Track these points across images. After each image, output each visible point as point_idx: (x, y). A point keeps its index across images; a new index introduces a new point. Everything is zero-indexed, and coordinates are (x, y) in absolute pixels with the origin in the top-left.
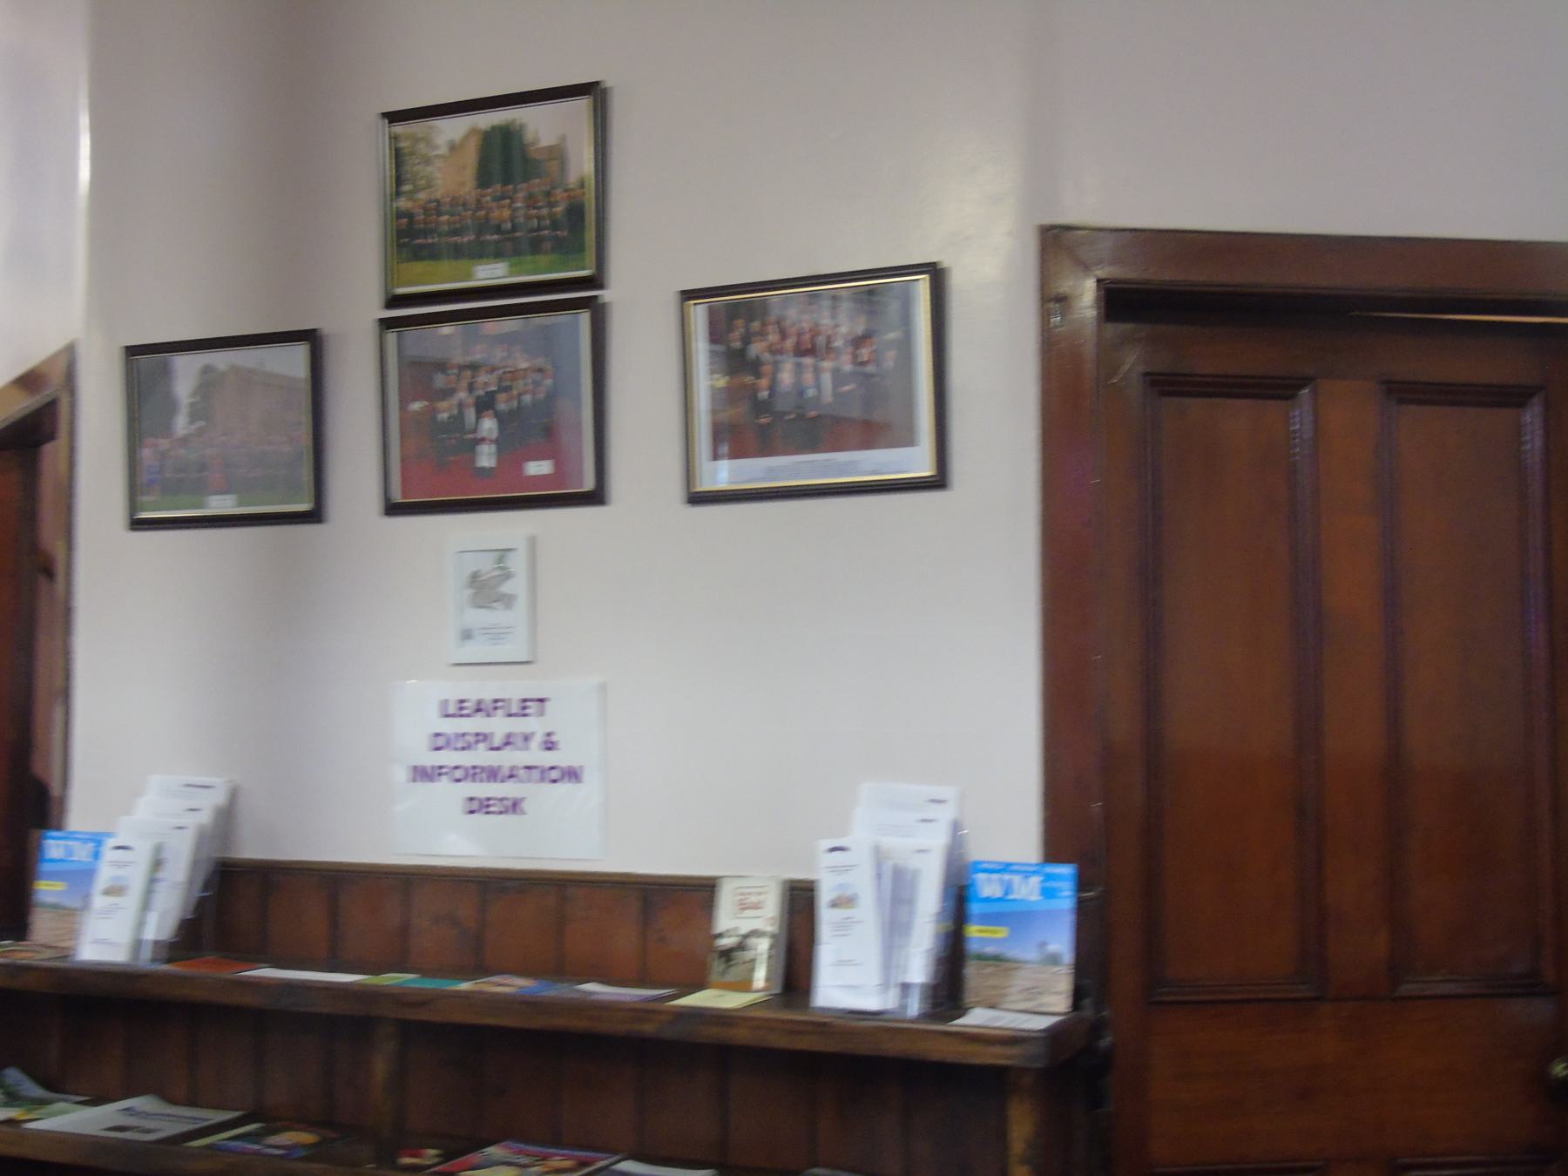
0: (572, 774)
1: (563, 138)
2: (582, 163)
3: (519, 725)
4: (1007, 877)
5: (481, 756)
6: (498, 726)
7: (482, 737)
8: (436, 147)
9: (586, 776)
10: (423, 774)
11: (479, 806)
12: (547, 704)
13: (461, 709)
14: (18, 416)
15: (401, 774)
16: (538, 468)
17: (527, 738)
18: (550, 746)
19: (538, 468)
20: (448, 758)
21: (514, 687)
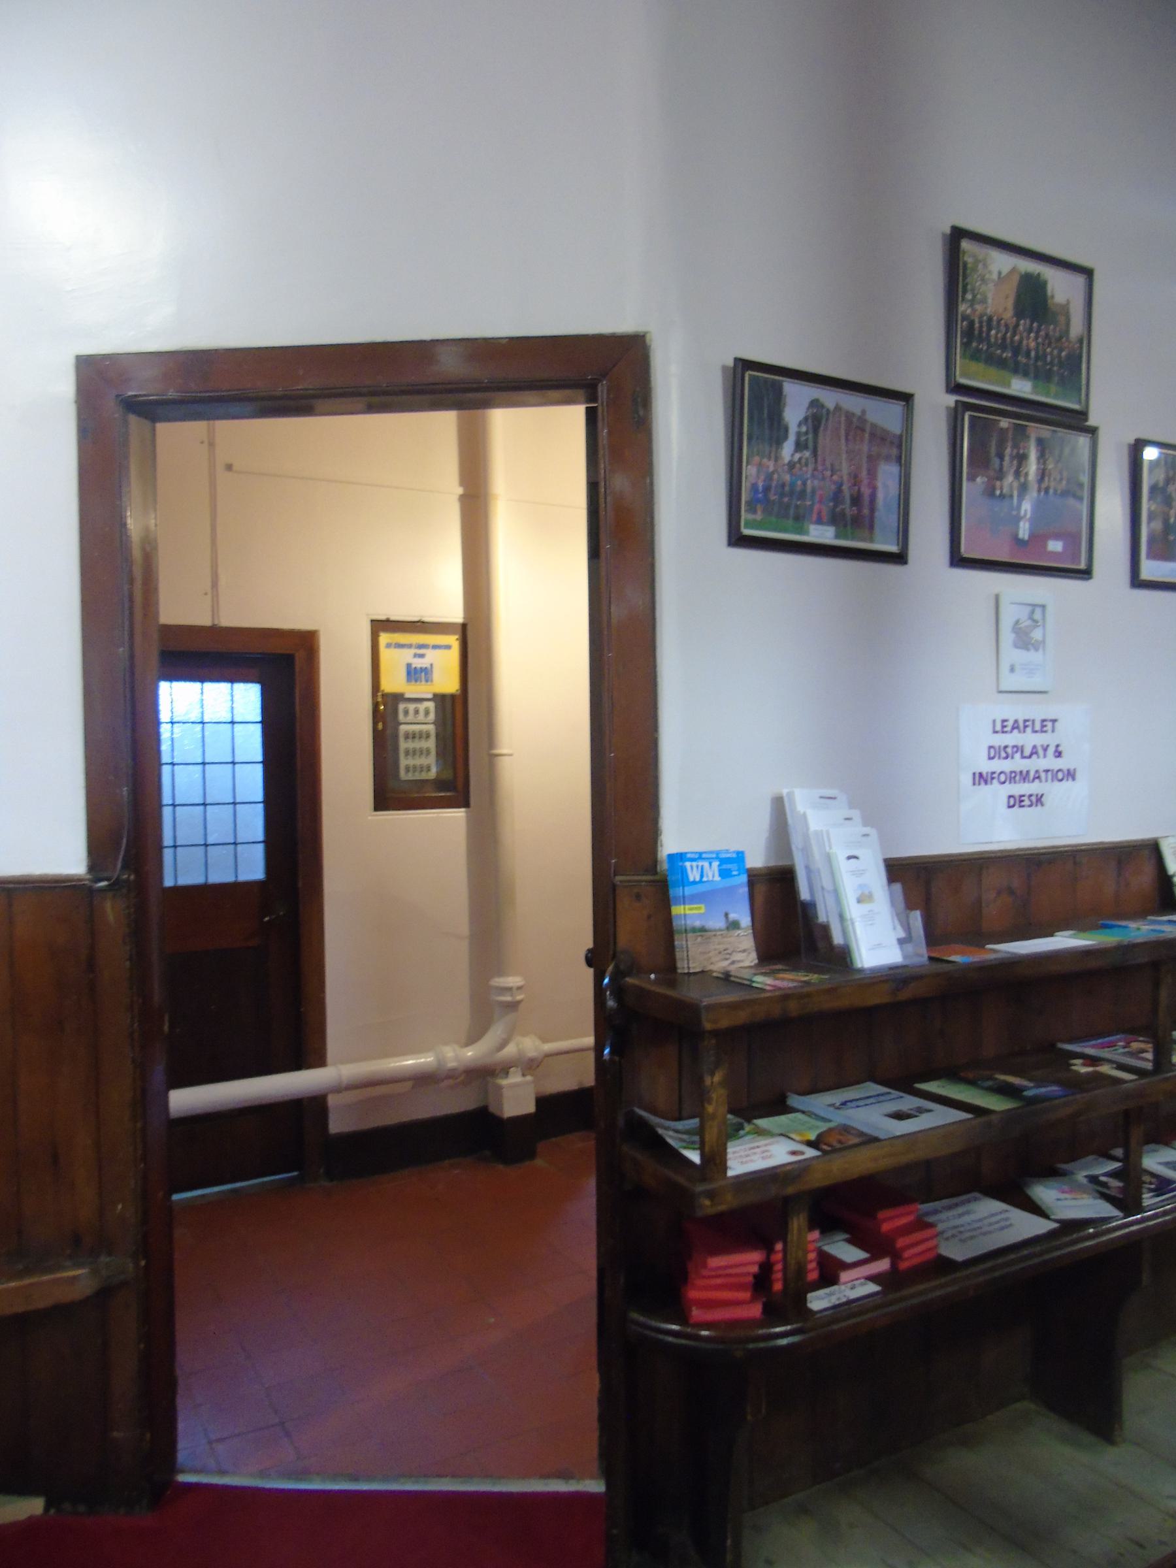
0: (1071, 775)
1: (1068, 302)
2: (1076, 328)
3: (1039, 740)
4: (700, 864)
5: (1017, 764)
6: (1029, 740)
7: (1019, 749)
8: (990, 272)
9: (1078, 775)
10: (981, 779)
11: (1016, 802)
12: (1057, 724)
13: (1003, 727)
14: (654, 405)
15: (966, 779)
16: (1055, 546)
17: (1045, 749)
18: (1058, 754)
19: (1055, 546)
20: (998, 765)
21: (1036, 711)
